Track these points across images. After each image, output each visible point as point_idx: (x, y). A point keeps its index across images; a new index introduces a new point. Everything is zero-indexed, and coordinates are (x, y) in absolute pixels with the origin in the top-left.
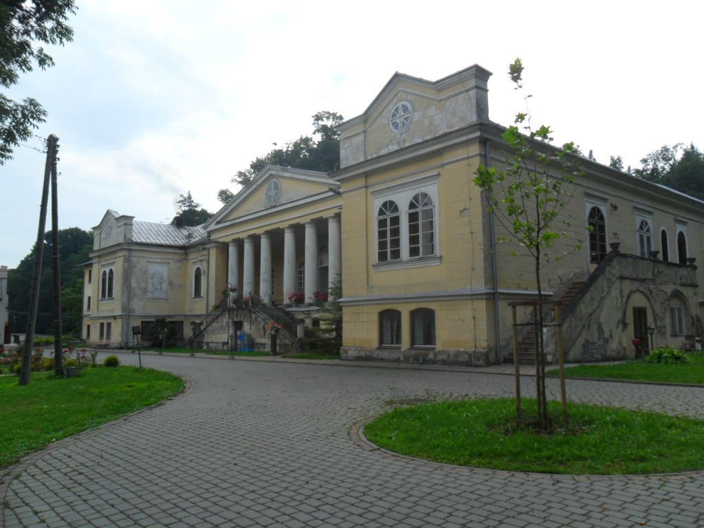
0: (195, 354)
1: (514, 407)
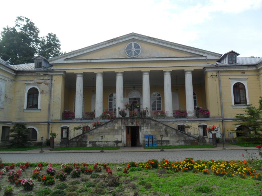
0: (43, 150)
1: (222, 140)
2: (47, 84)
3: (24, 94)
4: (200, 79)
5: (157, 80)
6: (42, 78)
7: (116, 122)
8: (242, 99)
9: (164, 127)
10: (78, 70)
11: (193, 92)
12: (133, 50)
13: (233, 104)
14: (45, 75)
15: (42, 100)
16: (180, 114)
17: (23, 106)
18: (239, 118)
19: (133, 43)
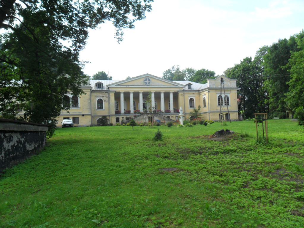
2: (107, 97)
3: (96, 102)
4: (176, 95)
5: (158, 95)
6: (104, 94)
7: (144, 115)
8: (193, 105)
9: (163, 117)
10: (122, 90)
11: (134, 101)
12: (147, 81)
13: (97, 108)
14: (106, 93)
15: (105, 105)
16: (168, 111)
17: (96, 108)
18: (191, 113)
19: (147, 78)
